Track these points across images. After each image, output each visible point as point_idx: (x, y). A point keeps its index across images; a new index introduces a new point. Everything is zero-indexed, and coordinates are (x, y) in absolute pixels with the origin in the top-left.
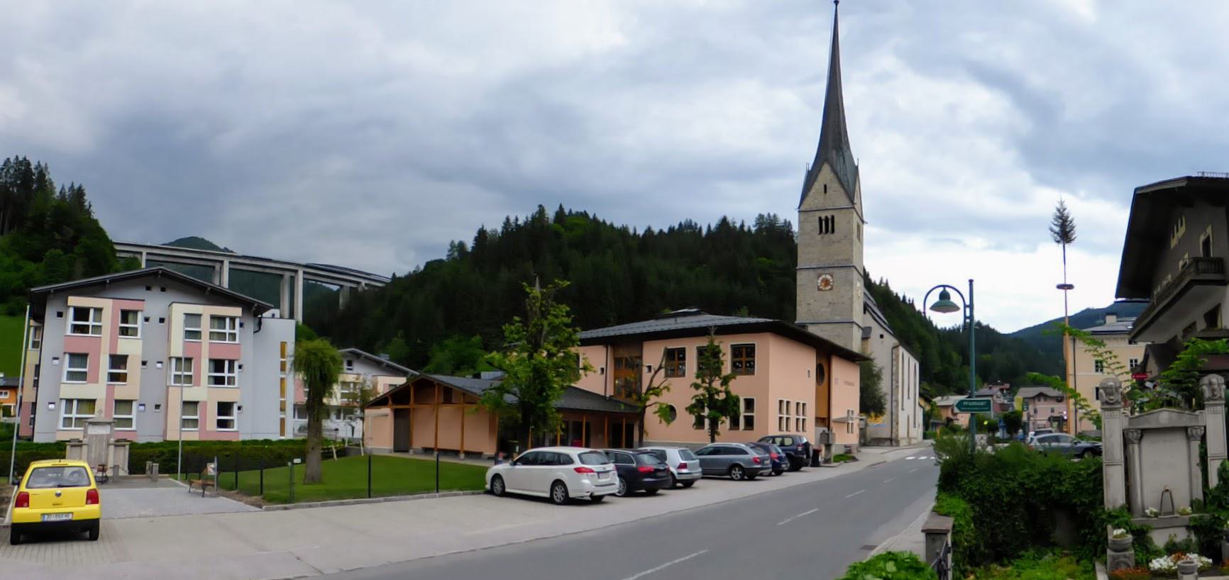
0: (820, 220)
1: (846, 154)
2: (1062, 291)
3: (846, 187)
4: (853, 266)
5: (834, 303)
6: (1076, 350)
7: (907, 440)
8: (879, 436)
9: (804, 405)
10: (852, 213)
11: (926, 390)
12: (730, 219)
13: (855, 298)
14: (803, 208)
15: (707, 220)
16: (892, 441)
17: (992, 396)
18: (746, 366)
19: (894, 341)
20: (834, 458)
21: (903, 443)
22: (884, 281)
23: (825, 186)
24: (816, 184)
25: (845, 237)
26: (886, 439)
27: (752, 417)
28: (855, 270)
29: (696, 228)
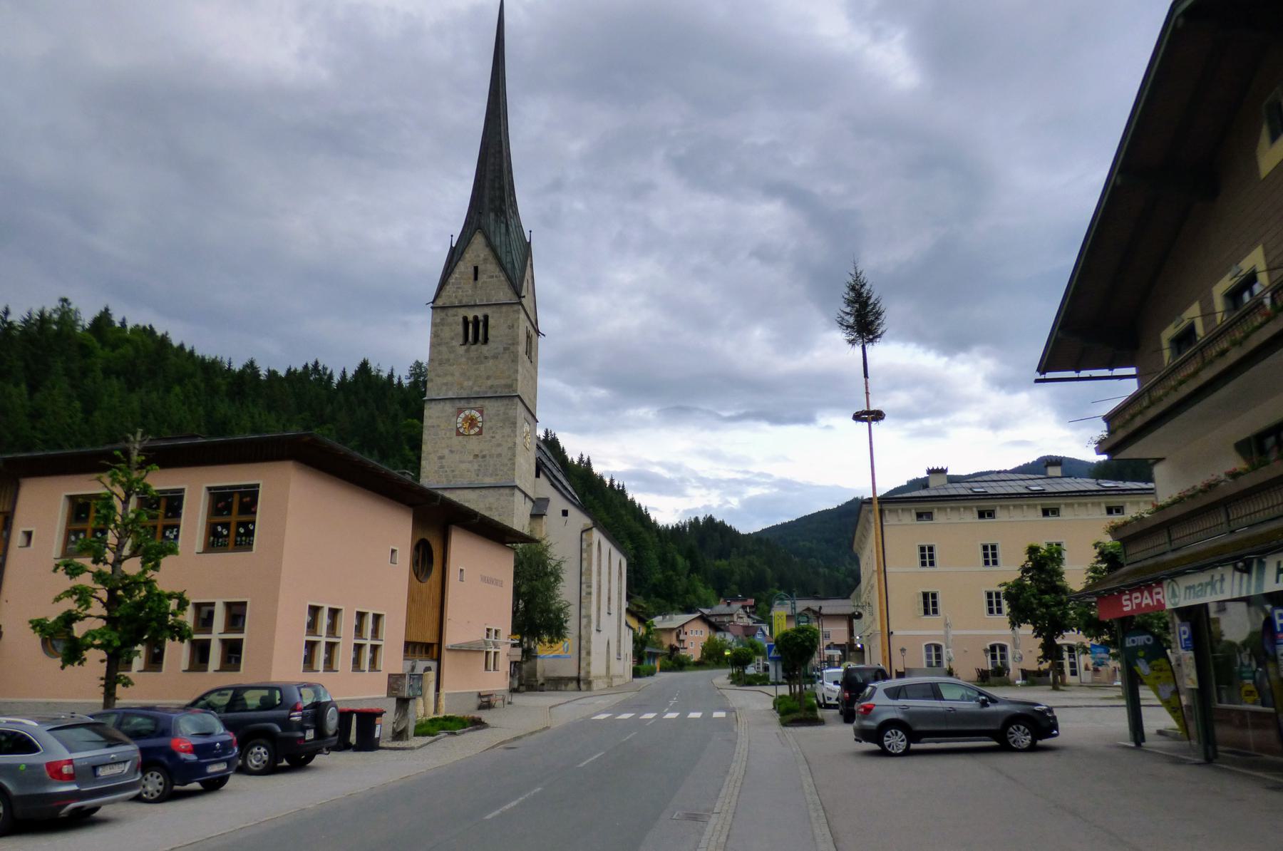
0: (465, 319)
1: (512, 222)
2: (874, 407)
3: (509, 272)
5: (484, 457)
6: (885, 528)
7: (606, 680)
8: (556, 674)
10: (518, 312)
11: (641, 607)
12: (373, 365)
13: (519, 448)
14: (440, 303)
15: (341, 365)
16: (580, 682)
17: (731, 615)
18: (238, 534)
19: (586, 521)
20: (417, 727)
21: (598, 685)
22: (585, 459)
23: (476, 269)
24: (461, 264)
25: (505, 349)
26: (570, 679)
27: (241, 641)
28: (520, 404)
29: (325, 374)
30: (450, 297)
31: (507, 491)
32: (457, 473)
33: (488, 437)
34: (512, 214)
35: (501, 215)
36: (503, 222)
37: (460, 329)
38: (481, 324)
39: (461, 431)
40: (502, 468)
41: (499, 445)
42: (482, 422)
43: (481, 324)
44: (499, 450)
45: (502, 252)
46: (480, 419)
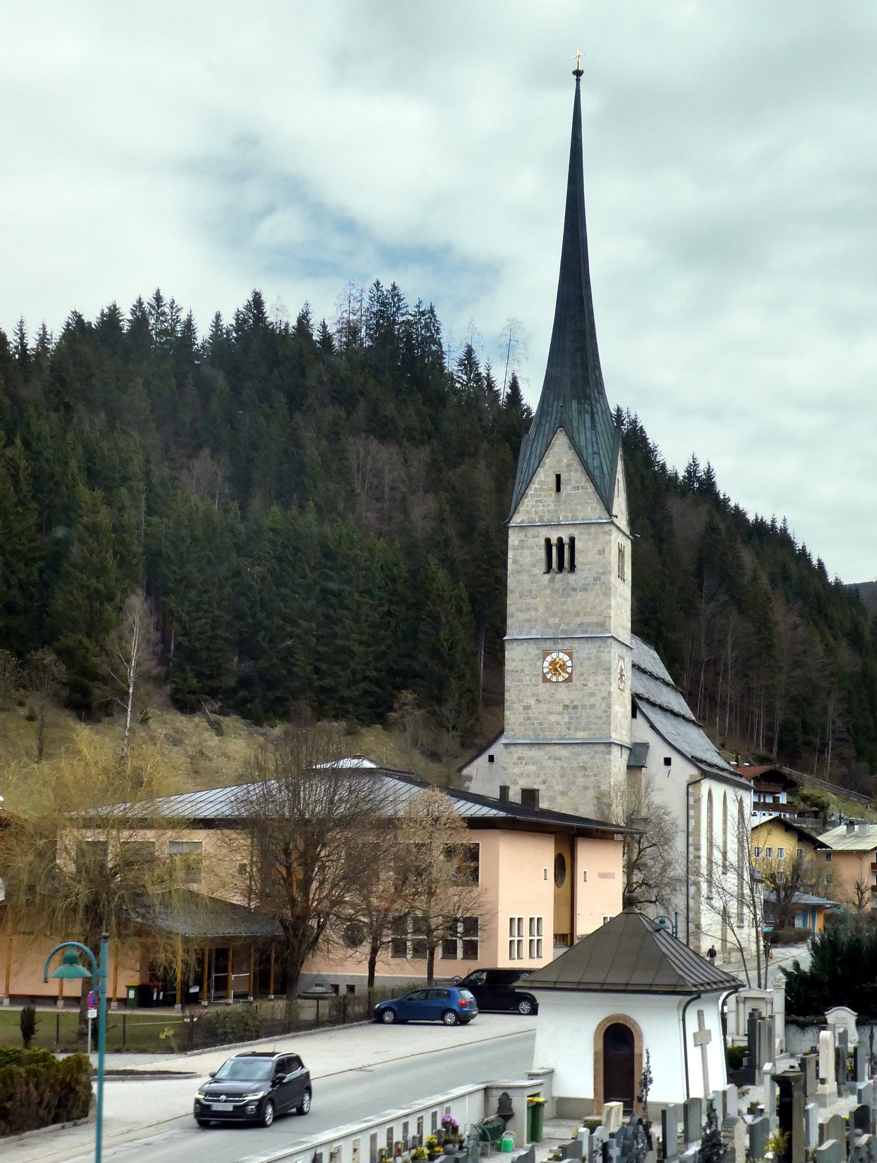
0: (548, 541)
3: (598, 480)
4: (612, 637)
5: (575, 707)
9: (539, 919)
10: (609, 533)
23: (558, 477)
25: (595, 579)
29: (176, 321)
30: (528, 512)
31: (602, 748)
32: (545, 725)
33: (579, 685)
34: (597, 395)
35: (585, 403)
36: (587, 412)
37: (542, 553)
38: (566, 547)
39: (548, 677)
40: (595, 721)
41: (592, 695)
42: (572, 667)
43: (566, 547)
44: (592, 700)
45: (588, 453)
46: (569, 664)
